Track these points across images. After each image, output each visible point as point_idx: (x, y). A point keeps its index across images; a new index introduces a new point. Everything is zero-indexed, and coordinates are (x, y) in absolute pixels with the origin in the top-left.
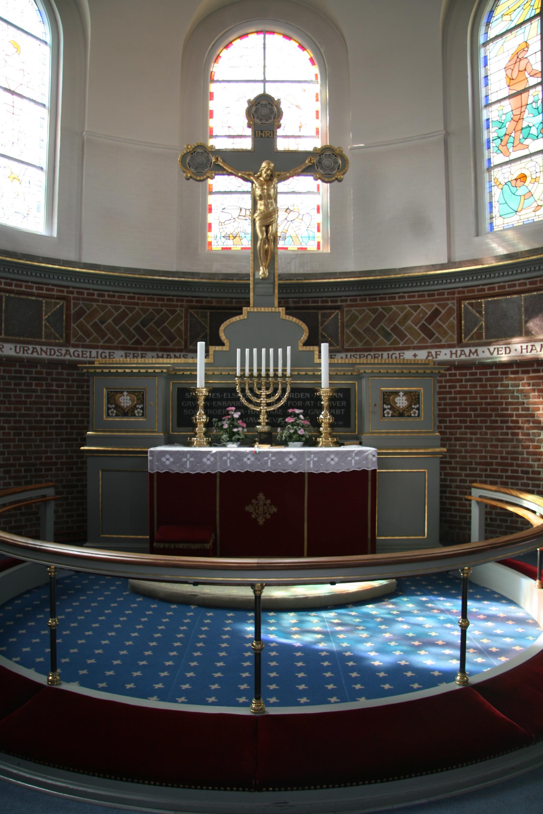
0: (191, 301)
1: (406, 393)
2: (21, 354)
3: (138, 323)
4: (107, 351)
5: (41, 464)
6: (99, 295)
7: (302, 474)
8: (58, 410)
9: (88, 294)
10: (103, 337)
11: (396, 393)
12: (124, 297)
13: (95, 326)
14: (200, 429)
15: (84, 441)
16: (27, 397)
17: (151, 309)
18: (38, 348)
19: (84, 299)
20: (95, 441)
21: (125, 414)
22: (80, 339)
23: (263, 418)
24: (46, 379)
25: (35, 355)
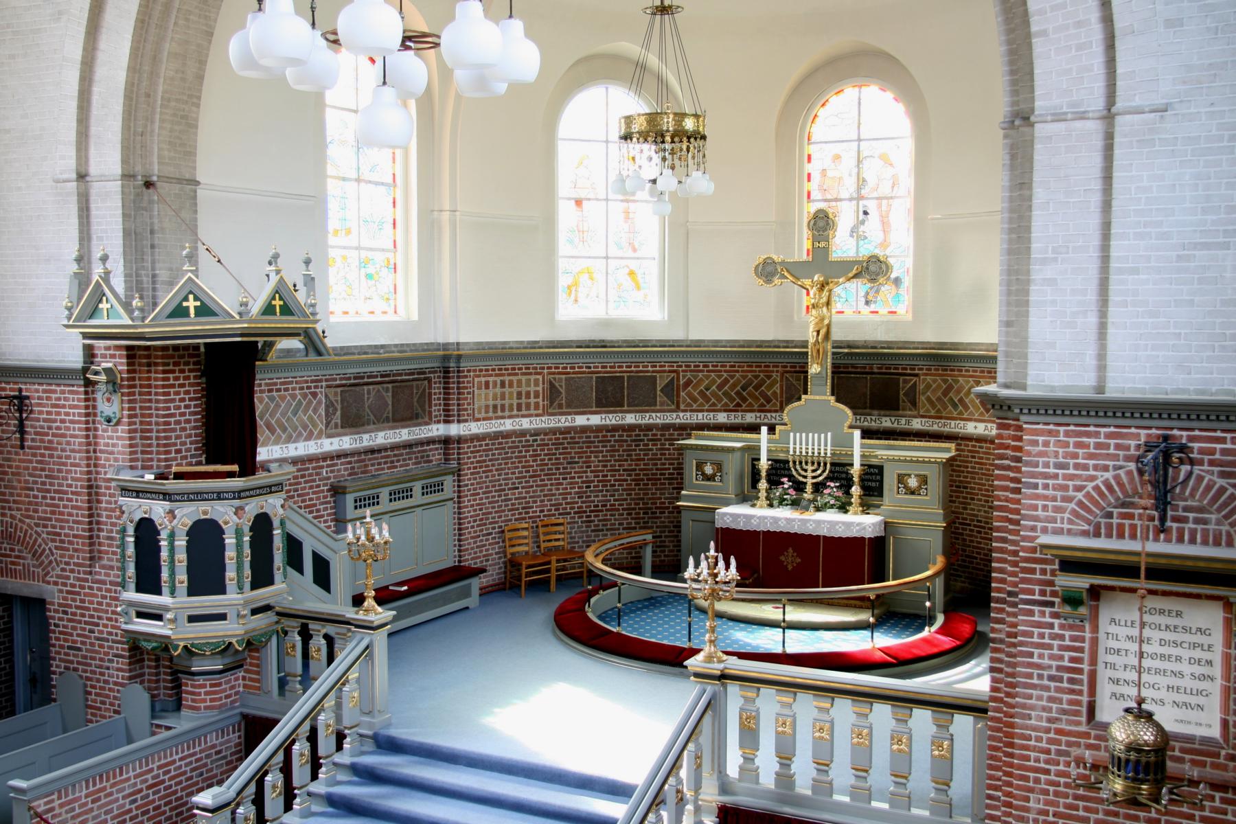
0: (786, 367)
1: (916, 476)
2: (640, 422)
3: (739, 388)
4: (712, 414)
5: (656, 508)
6: (704, 366)
7: (818, 537)
8: (670, 464)
9: (695, 366)
10: (707, 402)
11: (909, 475)
12: (726, 366)
13: (702, 393)
14: (763, 494)
15: (678, 499)
16: (645, 455)
17: (750, 375)
18: (654, 415)
19: (691, 371)
20: (689, 498)
21: (709, 479)
22: (689, 405)
23: (809, 488)
24: (660, 440)
25: (651, 421)
